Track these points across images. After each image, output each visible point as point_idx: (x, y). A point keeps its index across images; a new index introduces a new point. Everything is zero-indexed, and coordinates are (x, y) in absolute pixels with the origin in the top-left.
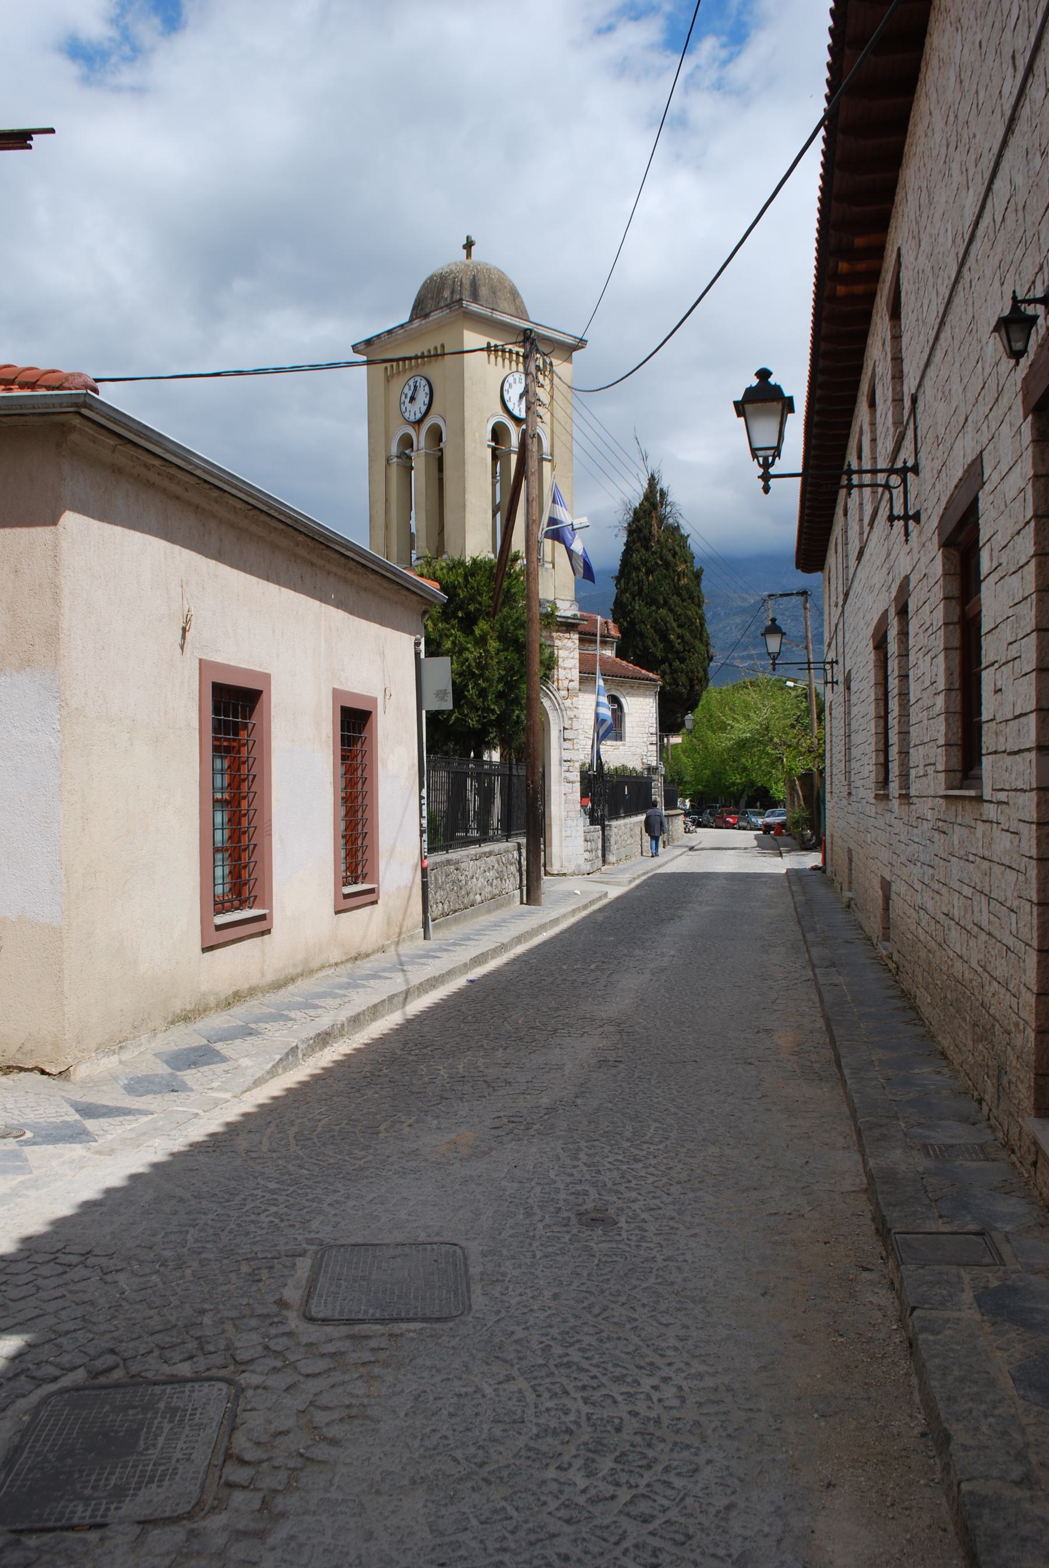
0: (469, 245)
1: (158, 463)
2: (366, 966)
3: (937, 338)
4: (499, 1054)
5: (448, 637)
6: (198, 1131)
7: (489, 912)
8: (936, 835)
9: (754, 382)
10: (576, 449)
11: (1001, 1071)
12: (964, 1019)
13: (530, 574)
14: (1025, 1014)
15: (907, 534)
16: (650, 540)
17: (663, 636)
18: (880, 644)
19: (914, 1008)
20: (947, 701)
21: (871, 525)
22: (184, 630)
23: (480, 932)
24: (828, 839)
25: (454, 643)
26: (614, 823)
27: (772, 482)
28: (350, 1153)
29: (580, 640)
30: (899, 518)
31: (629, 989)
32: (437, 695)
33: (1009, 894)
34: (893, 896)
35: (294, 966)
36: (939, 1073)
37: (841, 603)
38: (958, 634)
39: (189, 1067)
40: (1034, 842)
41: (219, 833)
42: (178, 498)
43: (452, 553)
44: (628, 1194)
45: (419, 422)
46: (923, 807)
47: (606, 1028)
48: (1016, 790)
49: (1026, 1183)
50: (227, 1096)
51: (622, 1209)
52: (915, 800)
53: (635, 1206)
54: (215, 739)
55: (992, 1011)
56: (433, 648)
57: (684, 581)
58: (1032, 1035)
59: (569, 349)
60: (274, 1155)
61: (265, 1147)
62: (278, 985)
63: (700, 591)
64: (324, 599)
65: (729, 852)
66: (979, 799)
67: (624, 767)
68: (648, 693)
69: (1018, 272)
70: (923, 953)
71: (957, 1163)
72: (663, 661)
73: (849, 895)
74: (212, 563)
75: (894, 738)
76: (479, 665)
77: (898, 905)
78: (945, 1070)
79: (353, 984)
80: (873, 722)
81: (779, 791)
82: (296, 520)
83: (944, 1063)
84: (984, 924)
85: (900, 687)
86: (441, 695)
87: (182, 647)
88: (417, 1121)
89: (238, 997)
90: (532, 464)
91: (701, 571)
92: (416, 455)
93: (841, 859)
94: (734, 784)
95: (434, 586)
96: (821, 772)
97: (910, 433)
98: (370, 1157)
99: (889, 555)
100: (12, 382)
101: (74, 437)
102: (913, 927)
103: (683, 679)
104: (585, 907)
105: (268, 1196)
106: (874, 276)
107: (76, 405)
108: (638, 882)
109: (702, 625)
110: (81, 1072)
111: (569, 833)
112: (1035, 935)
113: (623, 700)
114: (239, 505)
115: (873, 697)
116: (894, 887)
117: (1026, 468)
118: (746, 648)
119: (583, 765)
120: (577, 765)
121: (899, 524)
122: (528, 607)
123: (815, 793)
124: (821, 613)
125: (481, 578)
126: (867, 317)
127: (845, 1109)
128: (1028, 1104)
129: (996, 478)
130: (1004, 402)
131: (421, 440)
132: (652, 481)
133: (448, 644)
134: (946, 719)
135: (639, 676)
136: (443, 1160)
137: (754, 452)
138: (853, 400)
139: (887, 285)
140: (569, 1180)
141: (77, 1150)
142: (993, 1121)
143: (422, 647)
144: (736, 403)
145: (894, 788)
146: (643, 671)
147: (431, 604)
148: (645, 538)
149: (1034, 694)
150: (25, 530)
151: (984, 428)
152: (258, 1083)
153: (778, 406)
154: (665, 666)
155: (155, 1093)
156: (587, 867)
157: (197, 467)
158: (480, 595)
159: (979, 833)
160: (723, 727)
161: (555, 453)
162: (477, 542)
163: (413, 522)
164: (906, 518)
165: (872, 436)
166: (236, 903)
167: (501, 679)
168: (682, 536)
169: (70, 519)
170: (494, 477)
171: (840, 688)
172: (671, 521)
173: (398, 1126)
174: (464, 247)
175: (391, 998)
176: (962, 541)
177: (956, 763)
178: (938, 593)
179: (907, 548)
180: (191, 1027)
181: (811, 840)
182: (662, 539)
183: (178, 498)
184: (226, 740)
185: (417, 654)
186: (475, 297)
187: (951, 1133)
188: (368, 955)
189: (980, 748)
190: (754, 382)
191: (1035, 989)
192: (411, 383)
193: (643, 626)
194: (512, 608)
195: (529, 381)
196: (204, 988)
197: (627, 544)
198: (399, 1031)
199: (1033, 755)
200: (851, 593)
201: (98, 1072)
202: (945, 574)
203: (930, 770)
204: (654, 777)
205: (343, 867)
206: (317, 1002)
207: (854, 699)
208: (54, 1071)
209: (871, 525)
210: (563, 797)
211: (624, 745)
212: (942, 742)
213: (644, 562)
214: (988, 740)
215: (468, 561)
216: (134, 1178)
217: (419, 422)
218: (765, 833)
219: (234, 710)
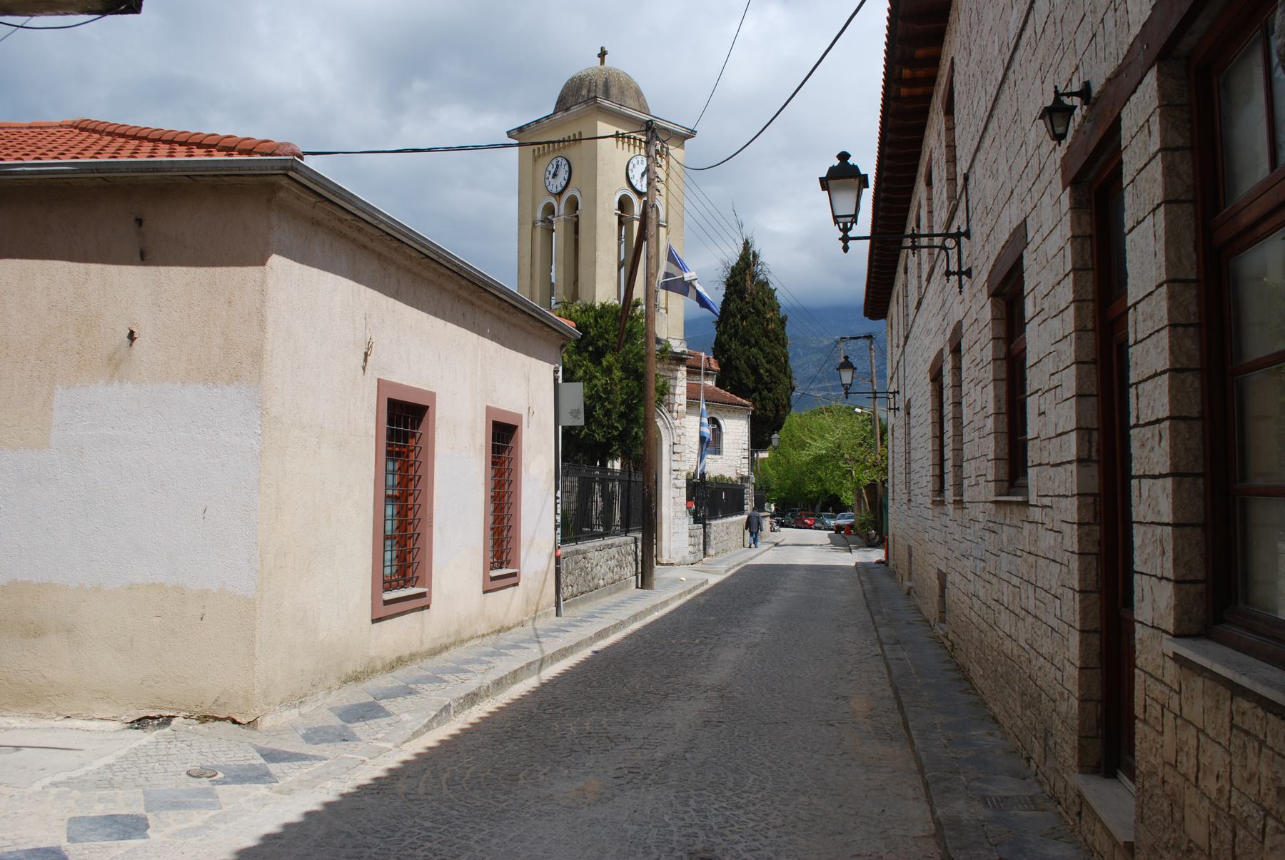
0: (603, 54)
1: (349, 217)
2: (508, 638)
3: (986, 128)
4: (620, 714)
5: (580, 367)
6: (364, 776)
7: (610, 594)
8: (987, 534)
9: (836, 162)
10: (687, 219)
11: (1047, 733)
12: (1013, 689)
13: (649, 316)
14: (1069, 685)
15: (961, 287)
17: (755, 370)
18: (937, 377)
19: (968, 679)
20: (996, 423)
21: (928, 280)
22: (366, 354)
23: (603, 611)
24: (890, 538)
25: (585, 372)
26: (713, 522)
27: (851, 243)
28: (494, 797)
29: (688, 372)
30: (954, 273)
31: (727, 661)
32: (571, 413)
33: (1053, 583)
34: (949, 585)
35: (448, 636)
36: (992, 735)
37: (902, 344)
38: (1004, 368)
39: (358, 720)
40: (1075, 539)
41: (389, 523)
42: (365, 247)
43: (584, 298)
44: (731, 837)
45: (560, 194)
46: (975, 511)
47: (710, 693)
48: (1059, 496)
49: (1072, 831)
50: (390, 745)
51: (727, 850)
52: (967, 505)
53: (738, 847)
54: (388, 445)
55: (1038, 683)
56: (568, 375)
58: (1076, 703)
59: (682, 137)
60: (429, 798)
61: (421, 791)
62: (434, 652)
64: (481, 333)
65: (807, 548)
66: (1026, 504)
67: (722, 477)
69: (1057, 72)
70: (976, 634)
71: (1012, 812)
72: (754, 391)
73: (910, 584)
74: (391, 300)
75: (948, 454)
76: (605, 391)
77: (952, 592)
78: (997, 733)
79: (497, 653)
80: (930, 442)
81: (848, 498)
82: (461, 268)
83: (996, 726)
84: (1031, 609)
85: (954, 412)
86: (574, 413)
87: (364, 369)
88: (551, 771)
89: (400, 661)
90: (651, 229)
92: (557, 220)
93: (902, 554)
94: (811, 492)
95: (570, 325)
96: (884, 482)
97: (962, 205)
98: (511, 801)
99: (944, 304)
100: (233, 149)
101: (282, 194)
102: (967, 612)
103: (770, 405)
104: (690, 591)
105: (424, 833)
106: (932, 80)
107: (284, 168)
108: (733, 571)
109: (786, 361)
110: (266, 722)
112: (1077, 618)
114: (414, 254)
115: (930, 420)
116: (949, 578)
117: (1065, 230)
118: (821, 381)
119: (689, 474)
120: (684, 474)
121: (954, 278)
122: (647, 344)
124: (884, 352)
125: (608, 320)
126: (924, 114)
127: (913, 765)
128: (1073, 762)
129: (1038, 239)
130: (1046, 177)
131: (561, 208)
132: (747, 245)
133: (580, 373)
134: (995, 438)
136: (573, 805)
137: (836, 218)
138: (912, 180)
139: (943, 87)
140: (681, 823)
141: (261, 789)
142: (1040, 777)
143: (560, 374)
144: (821, 179)
145: (949, 495)
147: (569, 340)
149: (1074, 416)
150: (238, 269)
151: (1028, 198)
152: (416, 735)
153: (855, 182)
154: (756, 395)
155: (329, 741)
156: (691, 559)
157: (382, 222)
158: (607, 333)
159: (1026, 532)
160: (803, 445)
162: (605, 291)
163: (553, 274)
164: (960, 273)
165: (929, 207)
166: (401, 582)
167: (623, 402)
169: (276, 261)
170: (619, 239)
171: (902, 413)
172: (761, 277)
173: (534, 774)
174: (599, 56)
175: (529, 664)
176: (1008, 293)
177: (1004, 474)
178: (988, 334)
179: (960, 298)
180: (361, 686)
183: (365, 247)
184: (399, 446)
185: (556, 380)
186: (607, 95)
187: (1005, 787)
188: (509, 629)
189: (1026, 461)
190: (836, 162)
191: (1078, 663)
192: (554, 162)
194: (633, 344)
196: (373, 653)
198: (535, 693)
199: (1074, 467)
200: (911, 336)
201: (280, 722)
202: (993, 319)
203: (981, 480)
205: (491, 554)
206: (466, 667)
207: (913, 422)
208: (244, 721)
209: (928, 280)
212: (991, 456)
213: (740, 310)
214: (1033, 455)
215: (598, 305)
216: (309, 814)
217: (560, 194)
219: (405, 421)
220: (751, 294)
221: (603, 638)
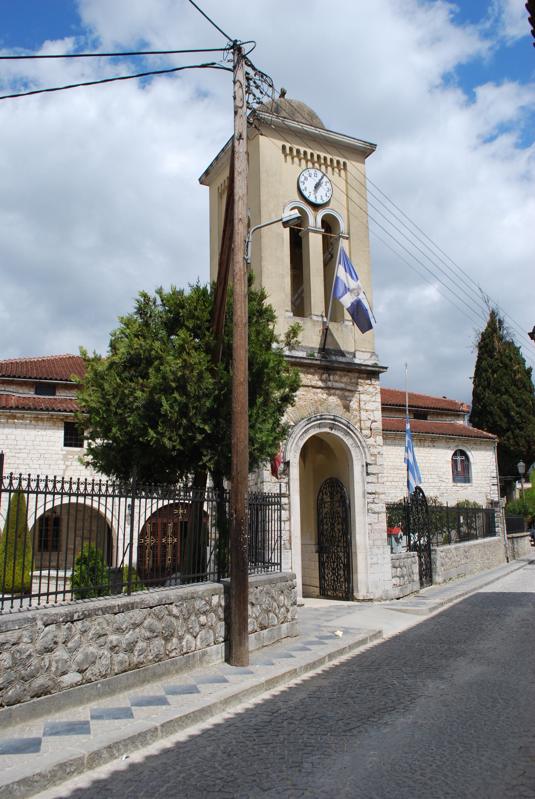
16: (493, 352)
17: (506, 413)
57: (518, 376)
63: (531, 382)
72: (507, 430)
91: (530, 369)
103: (522, 442)
111: (375, 560)
113: (469, 453)
132: (493, 314)
135: (482, 436)
146: (485, 433)
148: (490, 351)
154: (509, 434)
161: (351, 232)
172: (508, 339)
182: (502, 350)
193: (492, 407)
195: (236, 88)
204: (497, 509)
210: (368, 527)
211: (471, 486)
213: (490, 366)
220: (499, 352)
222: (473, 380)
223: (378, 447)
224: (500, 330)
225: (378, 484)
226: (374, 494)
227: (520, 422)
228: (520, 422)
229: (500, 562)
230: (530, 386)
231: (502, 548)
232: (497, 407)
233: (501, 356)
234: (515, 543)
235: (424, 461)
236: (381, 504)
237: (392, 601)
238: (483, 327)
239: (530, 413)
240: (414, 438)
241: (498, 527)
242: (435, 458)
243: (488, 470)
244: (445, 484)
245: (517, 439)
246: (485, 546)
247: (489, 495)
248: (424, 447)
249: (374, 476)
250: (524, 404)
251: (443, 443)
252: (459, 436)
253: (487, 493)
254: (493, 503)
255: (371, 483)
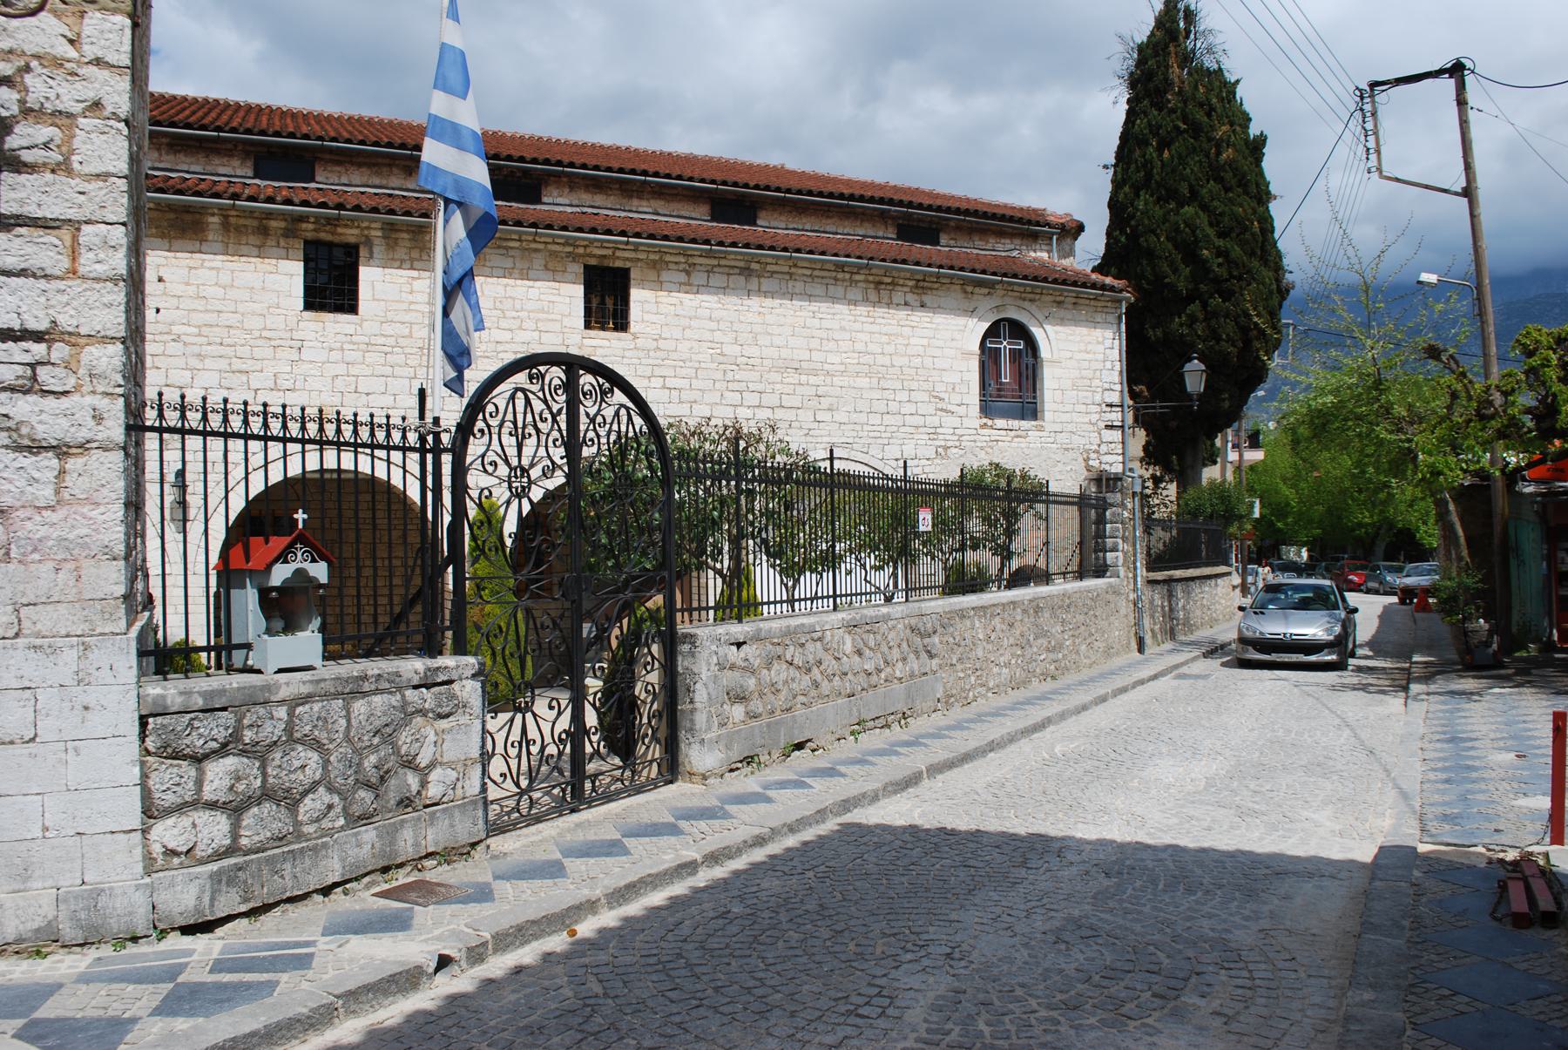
17: (1190, 252)
63: (1261, 174)
68: (1099, 318)
72: (1190, 299)
81: (1430, 535)
91: (1261, 141)
94: (1360, 525)
103: (1228, 329)
104: (760, 841)
113: (1037, 332)
123: (1498, 529)
154: (1195, 307)
168: (1225, 83)
181: (1488, 644)
197: (1129, 113)
213: (1154, 129)
218: (1402, 602)
221: (230, 971)
222: (1112, 171)
223: (92, 70)
224: (1187, 37)
225: (76, 286)
226: (38, 337)
227: (1225, 275)
228: (1225, 275)
229: (1108, 652)
230: (1257, 185)
231: (1123, 611)
232: (1168, 238)
233: (1185, 102)
234: (1180, 595)
235: (890, 349)
236: (89, 400)
237: (132, 949)
238: (1142, 26)
239: (1252, 254)
240: (857, 277)
241: (1114, 549)
242: (925, 342)
243: (1096, 382)
244: (955, 422)
245: (1213, 322)
246: (1038, 610)
247: (1093, 456)
248: (889, 305)
249: (51, 238)
250: (1237, 231)
251: (954, 296)
252: (1005, 275)
253: (1087, 451)
254: (1106, 482)
255: (23, 273)
